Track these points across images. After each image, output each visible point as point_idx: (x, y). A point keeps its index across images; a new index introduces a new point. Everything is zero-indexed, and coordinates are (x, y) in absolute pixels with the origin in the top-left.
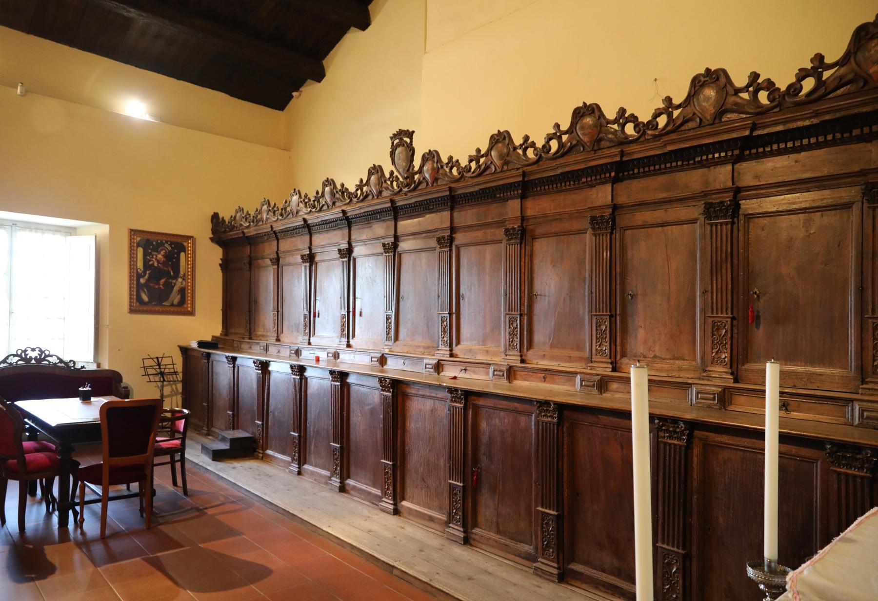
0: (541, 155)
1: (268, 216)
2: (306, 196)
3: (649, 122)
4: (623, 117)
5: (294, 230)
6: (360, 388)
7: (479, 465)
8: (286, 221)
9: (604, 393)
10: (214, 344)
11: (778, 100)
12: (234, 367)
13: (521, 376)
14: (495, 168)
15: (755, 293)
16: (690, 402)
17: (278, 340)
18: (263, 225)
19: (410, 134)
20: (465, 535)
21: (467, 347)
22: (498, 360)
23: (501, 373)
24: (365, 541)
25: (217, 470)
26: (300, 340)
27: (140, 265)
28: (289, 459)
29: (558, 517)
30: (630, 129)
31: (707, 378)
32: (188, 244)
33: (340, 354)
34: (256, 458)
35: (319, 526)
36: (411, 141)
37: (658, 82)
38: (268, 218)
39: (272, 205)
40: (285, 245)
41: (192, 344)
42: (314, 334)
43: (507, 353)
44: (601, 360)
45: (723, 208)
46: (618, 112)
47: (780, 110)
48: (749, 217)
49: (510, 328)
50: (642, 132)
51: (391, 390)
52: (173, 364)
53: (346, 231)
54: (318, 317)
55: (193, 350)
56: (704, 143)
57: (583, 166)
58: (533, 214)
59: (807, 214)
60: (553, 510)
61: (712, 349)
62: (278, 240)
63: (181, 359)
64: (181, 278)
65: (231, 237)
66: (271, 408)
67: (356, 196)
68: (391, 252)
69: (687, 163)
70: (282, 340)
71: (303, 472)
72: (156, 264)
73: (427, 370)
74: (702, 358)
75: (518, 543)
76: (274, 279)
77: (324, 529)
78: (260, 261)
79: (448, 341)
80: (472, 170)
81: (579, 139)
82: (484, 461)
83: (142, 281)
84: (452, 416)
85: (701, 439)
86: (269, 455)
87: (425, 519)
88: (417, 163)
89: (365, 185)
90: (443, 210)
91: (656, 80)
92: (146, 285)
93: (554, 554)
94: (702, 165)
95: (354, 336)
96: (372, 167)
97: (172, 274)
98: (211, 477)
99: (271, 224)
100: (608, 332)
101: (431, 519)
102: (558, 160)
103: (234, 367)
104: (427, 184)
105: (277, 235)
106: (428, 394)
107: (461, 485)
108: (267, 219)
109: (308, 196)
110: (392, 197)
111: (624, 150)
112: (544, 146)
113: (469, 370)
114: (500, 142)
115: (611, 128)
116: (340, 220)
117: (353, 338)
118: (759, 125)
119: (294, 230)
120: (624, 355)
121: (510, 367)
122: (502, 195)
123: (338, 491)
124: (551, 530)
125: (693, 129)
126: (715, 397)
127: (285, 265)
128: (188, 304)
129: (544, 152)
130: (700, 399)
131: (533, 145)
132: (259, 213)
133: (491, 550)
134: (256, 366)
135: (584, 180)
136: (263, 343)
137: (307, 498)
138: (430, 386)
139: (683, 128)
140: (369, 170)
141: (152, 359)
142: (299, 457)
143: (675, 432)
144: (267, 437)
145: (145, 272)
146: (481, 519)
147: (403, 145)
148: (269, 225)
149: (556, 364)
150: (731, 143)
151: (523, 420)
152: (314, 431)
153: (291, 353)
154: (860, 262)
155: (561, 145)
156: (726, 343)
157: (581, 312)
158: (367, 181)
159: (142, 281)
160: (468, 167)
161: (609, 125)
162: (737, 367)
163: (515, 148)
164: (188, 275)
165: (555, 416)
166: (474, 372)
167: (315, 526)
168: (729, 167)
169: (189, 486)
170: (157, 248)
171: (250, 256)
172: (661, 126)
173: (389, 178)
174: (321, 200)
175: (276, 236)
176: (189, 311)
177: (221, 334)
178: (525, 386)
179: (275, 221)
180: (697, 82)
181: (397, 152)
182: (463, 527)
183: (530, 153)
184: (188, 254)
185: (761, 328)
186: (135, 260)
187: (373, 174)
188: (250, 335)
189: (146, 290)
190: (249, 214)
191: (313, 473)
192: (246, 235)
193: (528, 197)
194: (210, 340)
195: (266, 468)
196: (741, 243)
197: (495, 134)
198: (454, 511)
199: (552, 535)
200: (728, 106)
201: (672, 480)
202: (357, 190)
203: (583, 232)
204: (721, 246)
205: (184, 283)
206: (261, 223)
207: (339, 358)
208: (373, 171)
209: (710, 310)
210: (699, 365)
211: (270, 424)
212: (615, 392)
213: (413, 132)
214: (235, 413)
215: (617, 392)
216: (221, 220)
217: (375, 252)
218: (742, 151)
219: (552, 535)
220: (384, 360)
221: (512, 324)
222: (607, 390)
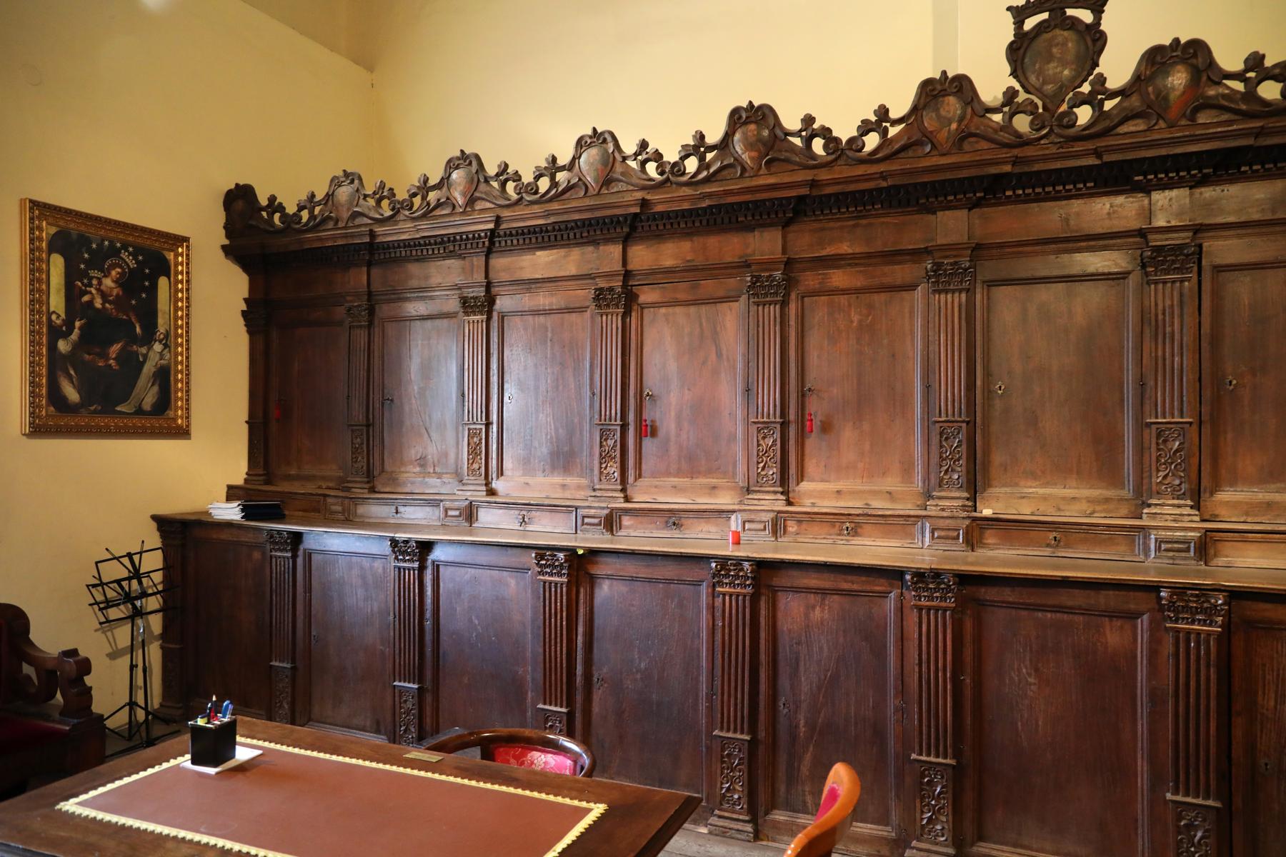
23: (761, 526)
27: (57, 302)
32: (177, 255)
41: (213, 512)
56: (1053, 167)
64: (160, 341)
72: (98, 303)
80: (415, 208)
83: (63, 346)
90: (608, 241)
92: (71, 357)
95: (501, 472)
97: (138, 330)
107: (416, 686)
117: (498, 478)
118: (505, 219)
130: (938, 538)
131: (658, 156)
139: (434, 213)
141: (117, 558)
145: (69, 323)
150: (1204, 156)
159: (63, 346)
161: (1225, 81)
163: (487, 181)
164: (177, 336)
170: (101, 259)
176: (179, 427)
178: (634, 536)
184: (177, 282)
186: (44, 287)
187: (457, 168)
188: (624, 490)
189: (72, 372)
197: (743, 108)
200: (973, 130)
203: (912, 287)
211: (596, 709)
215: (628, 527)
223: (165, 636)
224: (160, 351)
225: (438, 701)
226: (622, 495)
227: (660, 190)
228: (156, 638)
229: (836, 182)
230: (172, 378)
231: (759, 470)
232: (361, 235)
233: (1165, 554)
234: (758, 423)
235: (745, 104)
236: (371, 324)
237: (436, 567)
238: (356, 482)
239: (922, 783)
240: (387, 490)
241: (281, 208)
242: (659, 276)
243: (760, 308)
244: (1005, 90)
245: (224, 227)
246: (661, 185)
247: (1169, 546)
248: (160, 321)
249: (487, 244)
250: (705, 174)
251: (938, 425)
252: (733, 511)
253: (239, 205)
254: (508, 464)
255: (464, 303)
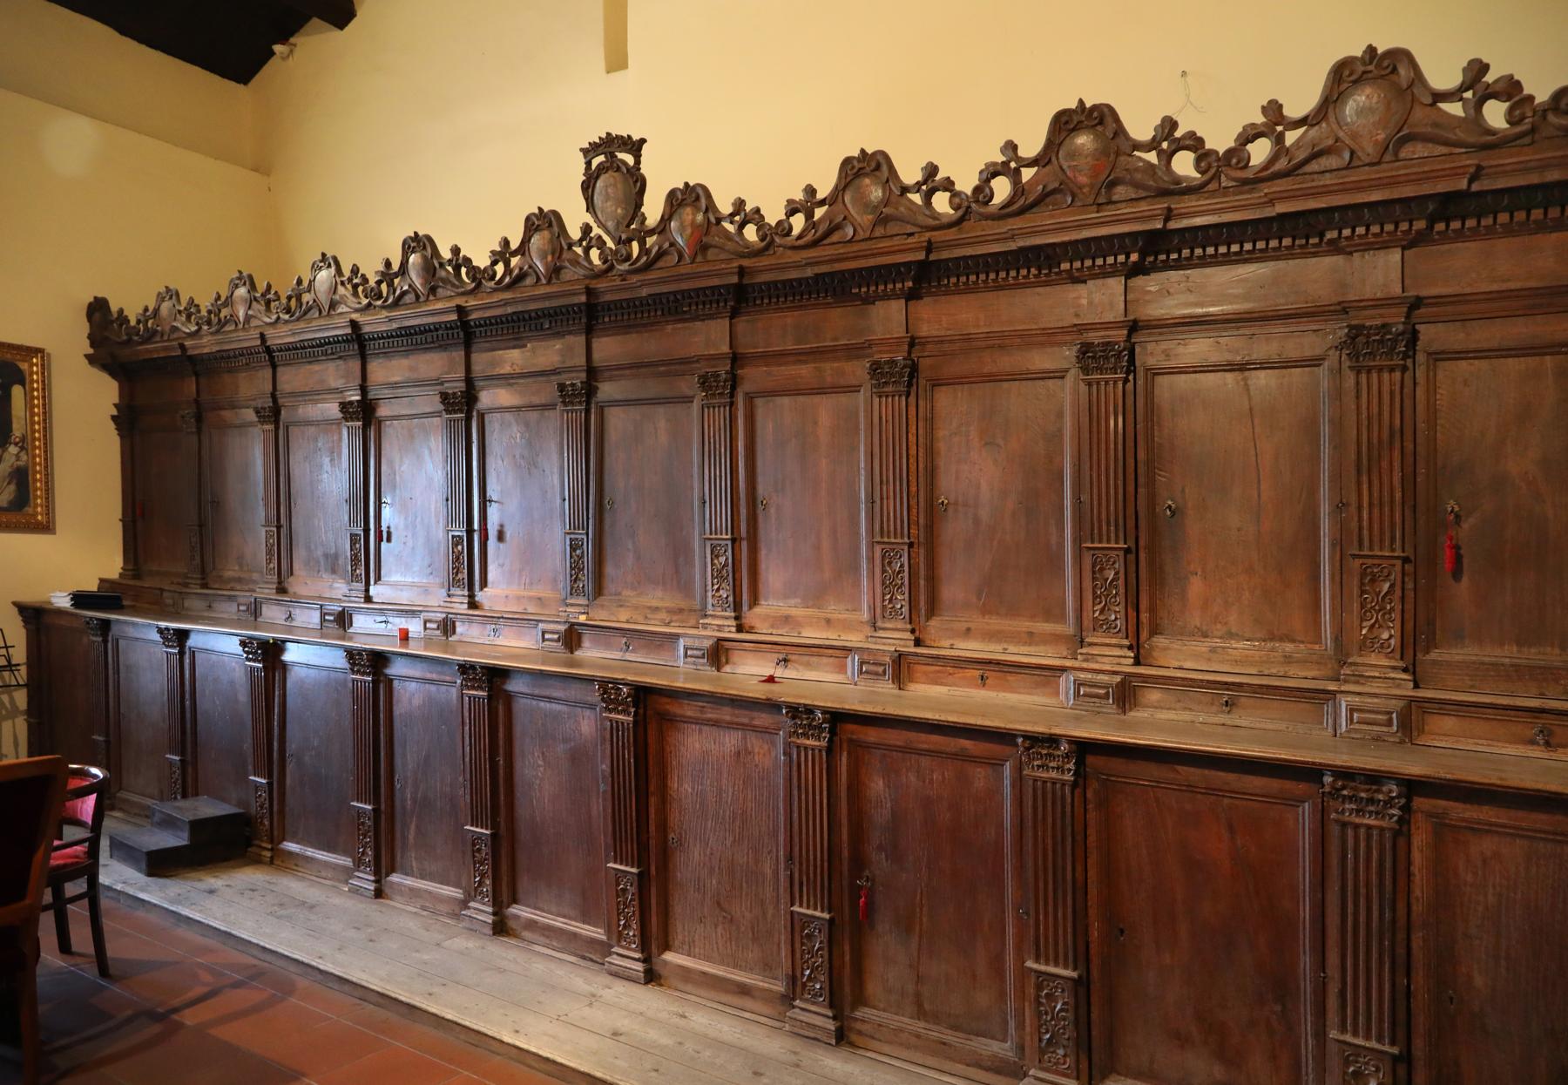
0: (969, 207)
1: (250, 312)
2: (355, 270)
3: (1230, 152)
4: (1168, 136)
5: (321, 345)
6: (542, 704)
7: (867, 873)
8: (302, 325)
9: (1131, 710)
10: (105, 598)
11: (1530, 120)
12: (182, 653)
13: (925, 673)
14: (855, 231)
15: (1170, 507)
16: (1330, 730)
17: (282, 590)
18: (235, 331)
19: (636, 147)
20: (838, 1024)
21: (498, 592)
22: (854, 639)
24: (618, 1062)
25: (172, 902)
26: (339, 590)
28: (347, 862)
29: (831, 921)
30: (1184, 164)
31: (1353, 678)
32: (32, 365)
33: (457, 624)
34: (257, 861)
35: (489, 1033)
36: (638, 162)
37: (1189, 78)
38: (252, 316)
39: (261, 287)
40: (292, 378)
41: (54, 600)
42: (378, 578)
43: (451, 592)
44: (1107, 641)
45: (1388, 337)
46: (734, 204)
47: (1533, 142)
48: (1154, 373)
49: (884, 571)
50: (1213, 171)
51: (633, 710)
52: (6, 647)
53: (355, 365)
54: (389, 540)
55: (60, 612)
57: (1534, 179)
58: (935, 333)
59: (1562, 356)
60: (1066, 967)
61: (1362, 620)
62: (274, 367)
63: (23, 632)
64: (16, 444)
65: (147, 356)
66: (292, 747)
67: (493, 277)
68: (580, 403)
69: (1304, 241)
70: (291, 590)
71: (387, 890)
73: (689, 659)
74: (1337, 640)
75: (972, 1037)
76: (266, 454)
77: (507, 1039)
78: (227, 414)
79: (731, 599)
81: (1064, 177)
82: (880, 863)
84: (794, 768)
85: (1429, 815)
86: (290, 854)
87: (727, 991)
88: (653, 209)
89: (514, 253)
91: (1184, 73)
93: (1068, 1060)
94: (1335, 248)
95: (484, 584)
96: (410, 238)
98: (152, 917)
99: (261, 330)
100: (1121, 582)
101: (744, 990)
102: (1011, 220)
103: (182, 653)
104: (681, 257)
105: (271, 356)
106: (728, 718)
108: (248, 318)
109: (361, 272)
110: (587, 282)
111: (1173, 206)
112: (977, 190)
113: (794, 661)
114: (866, 175)
115: (1140, 159)
116: (447, 328)
117: (375, 583)
119: (321, 345)
120: (1155, 631)
121: (900, 655)
122: (864, 290)
123: (491, 932)
124: (1061, 1010)
125: (1331, 171)
126: (1391, 720)
127: (298, 423)
128: (36, 506)
129: (977, 201)
131: (948, 185)
132: (225, 304)
133: (905, 1054)
134: (247, 653)
135: (1065, 266)
136: (245, 597)
137: (426, 957)
138: (732, 700)
139: (1308, 168)
140: (528, 219)
142: (377, 857)
143: (1371, 801)
144: (282, 812)
146: (873, 988)
147: (618, 169)
148: (255, 334)
149: (999, 648)
151: (980, 777)
152: (414, 800)
153: (323, 620)
154: (1077, 467)
155: (1018, 189)
156: (1392, 609)
157: (1054, 540)
158: (523, 243)
160: (786, 225)
161: (1135, 153)
162: (1415, 655)
164: (34, 439)
165: (1067, 766)
166: (808, 665)
167: (479, 1032)
168: (1395, 256)
169: (111, 951)
171: (197, 402)
172: (796, 231)
173: (581, 240)
174: (396, 281)
175: (272, 358)
176: (40, 523)
177: (120, 574)
178: (595, 656)
179: (271, 324)
180: (1347, 73)
181: (599, 184)
182: (831, 1006)
183: (941, 202)
184: (33, 390)
185: (1465, 579)
187: (538, 229)
190: (197, 306)
191: (414, 893)
192: (190, 352)
193: (921, 298)
194: (96, 589)
195: (291, 885)
196: (1420, 408)
197: (854, 157)
198: (808, 972)
199: (1064, 1019)
201: (1362, 901)
202: (494, 263)
204: (1380, 414)
205: (24, 457)
206: (228, 328)
207: (351, 624)
208: (413, 245)
209: (1356, 543)
210: (1330, 652)
211: (288, 781)
212: (1156, 708)
213: (643, 141)
214: (189, 758)
215: (1158, 707)
216: (115, 316)
217: (536, 400)
218: (1432, 221)
219: (1064, 1019)
220: (575, 638)
221: (890, 563)
222: (1135, 705)
223: (30, 712)
224: (16, 452)
225: (197, 774)
226: (734, 624)
227: (367, 312)
228: (22, 713)
229: (770, 269)
230: (30, 478)
231: (1097, 614)
232: (172, 348)
233: (1357, 726)
234: (884, 543)
235: (856, 153)
236: (199, 432)
237: (193, 654)
238: (192, 578)
239: (1345, 1073)
240: (216, 586)
241: (756, 216)
242: (1460, 307)
243: (1364, 377)
244: (1465, 64)
245: (88, 338)
246: (758, 253)
247: (1088, 690)
248: (15, 426)
249: (462, 334)
250: (1021, 202)
251: (1358, 562)
252: (1063, 669)
253: (97, 316)
254: (491, 576)
255: (343, 408)
